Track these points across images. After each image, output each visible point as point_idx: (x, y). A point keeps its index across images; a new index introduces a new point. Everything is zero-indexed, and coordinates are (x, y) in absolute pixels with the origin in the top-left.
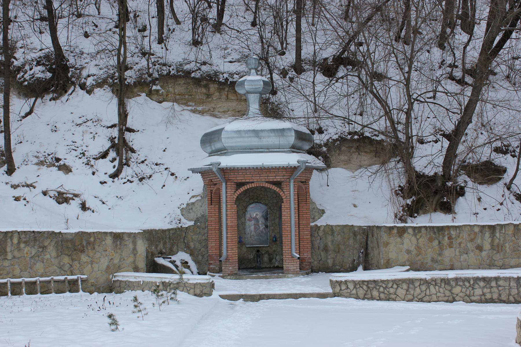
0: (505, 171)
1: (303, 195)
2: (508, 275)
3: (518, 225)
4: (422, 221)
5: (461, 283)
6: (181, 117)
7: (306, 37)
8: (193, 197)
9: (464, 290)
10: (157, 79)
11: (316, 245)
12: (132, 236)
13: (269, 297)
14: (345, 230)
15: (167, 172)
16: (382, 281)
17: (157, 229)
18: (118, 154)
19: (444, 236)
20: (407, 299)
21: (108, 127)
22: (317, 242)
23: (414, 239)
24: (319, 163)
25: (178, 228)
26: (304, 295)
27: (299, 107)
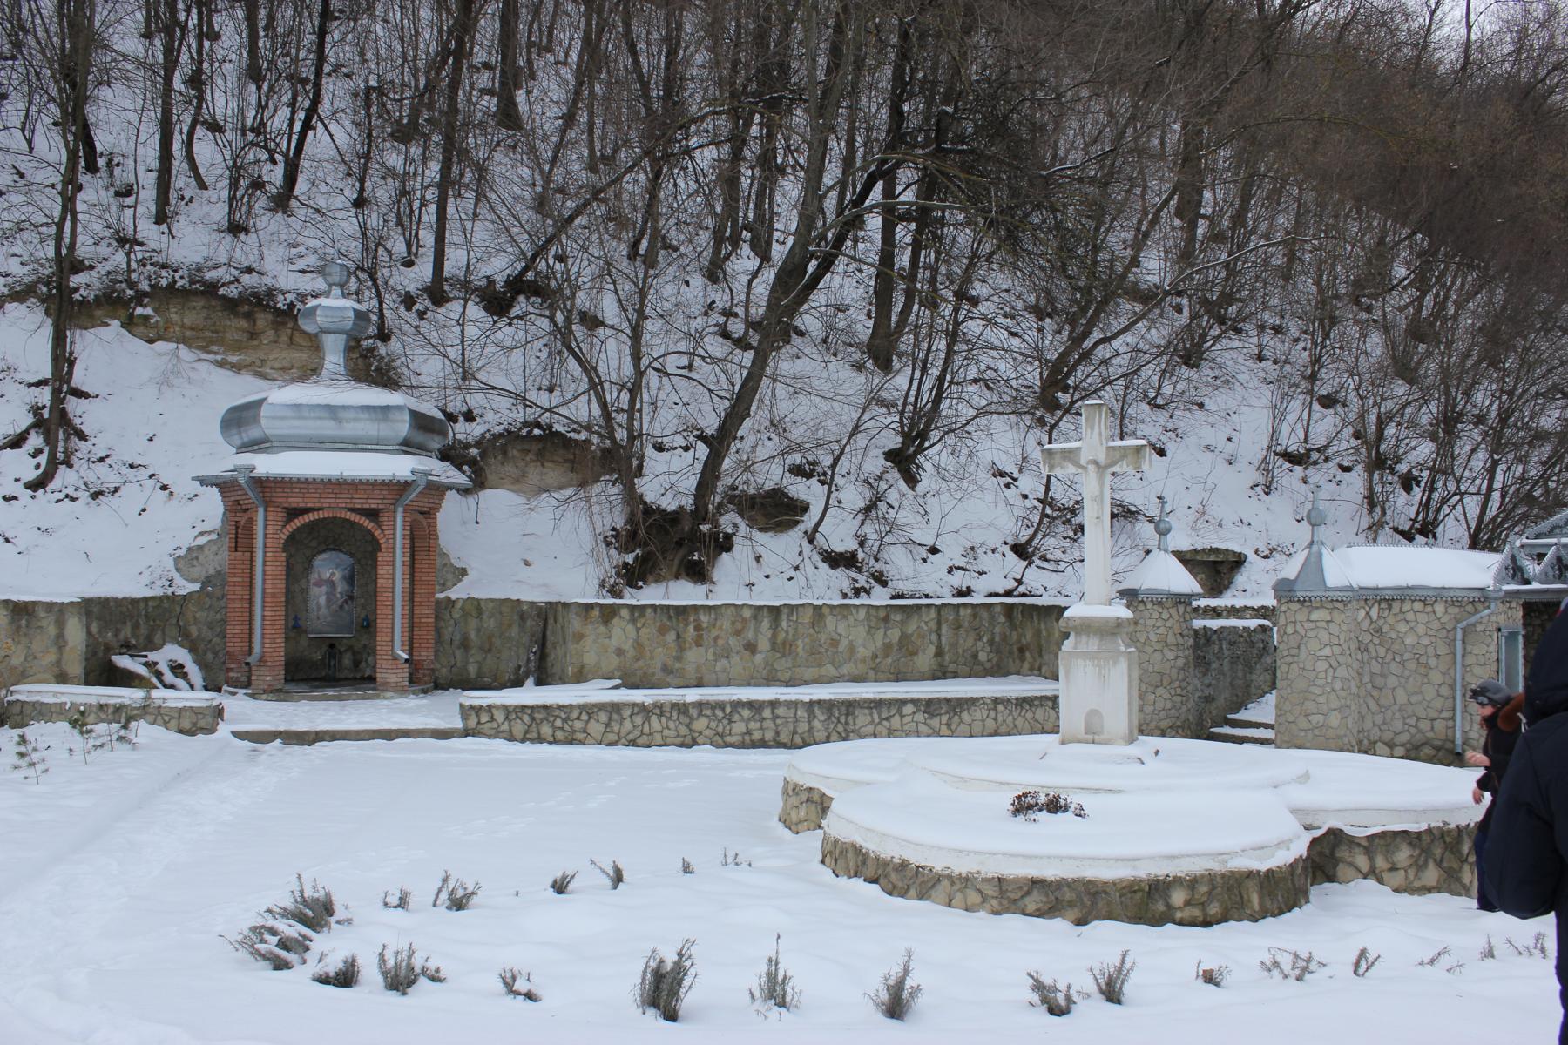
0: (805, 508)
1: (422, 539)
2: (793, 698)
3: (820, 607)
4: (650, 595)
5: (709, 712)
6: (192, 375)
7: (453, 235)
8: (202, 534)
9: (713, 724)
10: (146, 294)
11: (447, 638)
13: (334, 736)
14: (505, 609)
15: (152, 481)
16: (561, 707)
17: (120, 596)
18: (47, 441)
19: (687, 625)
20: (606, 741)
21: (30, 385)
22: (448, 631)
23: (630, 628)
24: (461, 479)
25: (167, 597)
26: (406, 734)
27: (430, 368)
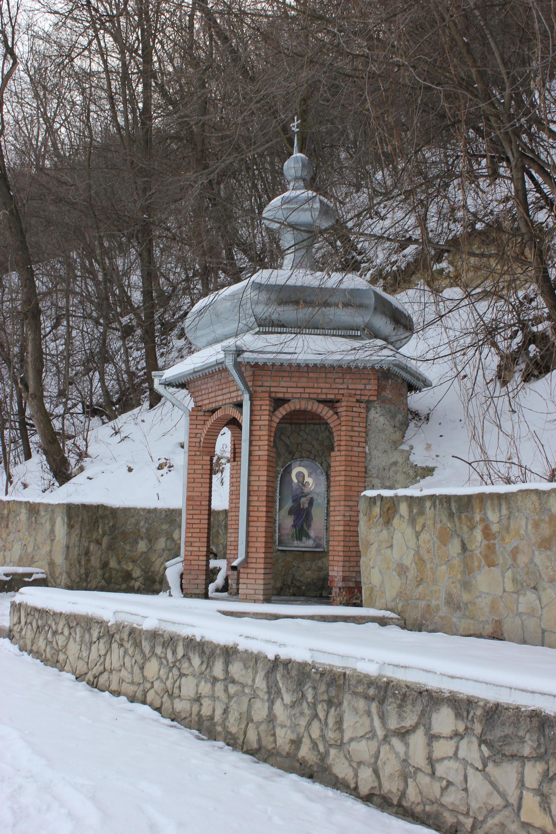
12: (50, 509)
19: (472, 528)
